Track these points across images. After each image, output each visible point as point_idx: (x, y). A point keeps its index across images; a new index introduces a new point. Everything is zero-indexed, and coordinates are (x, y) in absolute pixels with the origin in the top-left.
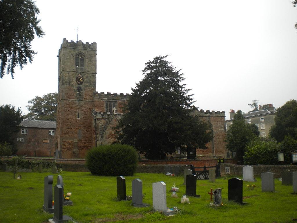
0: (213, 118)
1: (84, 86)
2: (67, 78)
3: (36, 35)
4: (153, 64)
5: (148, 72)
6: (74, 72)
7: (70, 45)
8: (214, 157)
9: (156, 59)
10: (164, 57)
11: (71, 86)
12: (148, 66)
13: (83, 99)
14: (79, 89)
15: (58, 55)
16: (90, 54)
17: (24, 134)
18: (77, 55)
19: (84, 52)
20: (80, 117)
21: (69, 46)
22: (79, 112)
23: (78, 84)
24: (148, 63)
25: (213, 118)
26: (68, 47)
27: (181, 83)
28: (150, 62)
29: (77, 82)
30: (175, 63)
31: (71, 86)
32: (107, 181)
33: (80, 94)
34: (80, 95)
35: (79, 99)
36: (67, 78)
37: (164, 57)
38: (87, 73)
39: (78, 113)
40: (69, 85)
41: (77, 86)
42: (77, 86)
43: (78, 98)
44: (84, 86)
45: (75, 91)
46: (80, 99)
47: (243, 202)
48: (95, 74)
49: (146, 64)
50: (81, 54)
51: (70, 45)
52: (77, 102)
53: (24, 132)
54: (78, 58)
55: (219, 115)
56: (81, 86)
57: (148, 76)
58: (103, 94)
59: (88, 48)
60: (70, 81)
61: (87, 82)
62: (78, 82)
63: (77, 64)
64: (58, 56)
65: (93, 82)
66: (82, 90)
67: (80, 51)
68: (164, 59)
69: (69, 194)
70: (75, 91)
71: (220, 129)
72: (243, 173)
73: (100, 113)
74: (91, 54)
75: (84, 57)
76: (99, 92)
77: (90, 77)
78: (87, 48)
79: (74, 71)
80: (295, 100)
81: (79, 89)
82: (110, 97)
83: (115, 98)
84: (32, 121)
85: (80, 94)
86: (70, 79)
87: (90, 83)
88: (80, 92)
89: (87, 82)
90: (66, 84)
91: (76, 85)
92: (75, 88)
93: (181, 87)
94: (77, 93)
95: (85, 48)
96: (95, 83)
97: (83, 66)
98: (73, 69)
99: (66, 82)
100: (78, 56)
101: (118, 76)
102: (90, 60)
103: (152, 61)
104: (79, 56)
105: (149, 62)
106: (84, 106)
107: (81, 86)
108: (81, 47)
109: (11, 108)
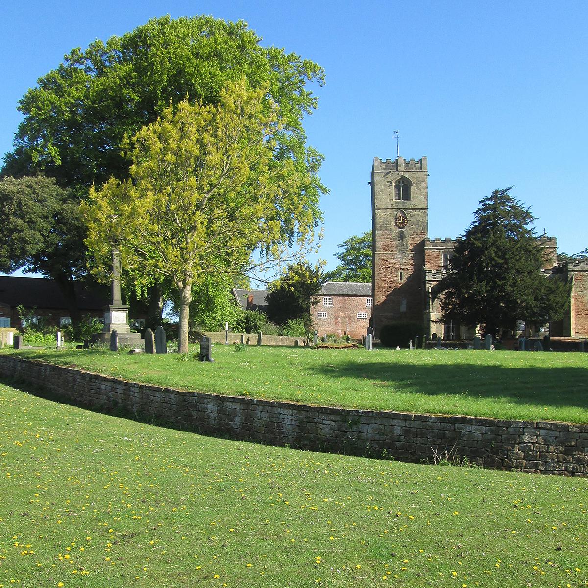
3: (95, 358)
7: (384, 167)
10: (506, 190)
13: (407, 251)
14: (402, 236)
17: (328, 305)
21: (384, 169)
23: (400, 228)
26: (383, 171)
28: (487, 199)
30: (521, 197)
32: (322, 386)
35: (401, 252)
36: (382, 220)
37: (506, 190)
40: (386, 230)
45: (394, 240)
46: (402, 251)
48: (426, 209)
49: (480, 202)
51: (384, 167)
52: (399, 256)
53: (328, 300)
56: (404, 230)
58: (438, 241)
62: (400, 225)
64: (369, 183)
65: (422, 223)
67: (402, 174)
81: (402, 236)
84: (340, 284)
88: (402, 240)
93: (528, 232)
95: (409, 169)
99: (381, 227)
101: (449, 219)
103: (489, 197)
104: (399, 182)
107: (404, 230)
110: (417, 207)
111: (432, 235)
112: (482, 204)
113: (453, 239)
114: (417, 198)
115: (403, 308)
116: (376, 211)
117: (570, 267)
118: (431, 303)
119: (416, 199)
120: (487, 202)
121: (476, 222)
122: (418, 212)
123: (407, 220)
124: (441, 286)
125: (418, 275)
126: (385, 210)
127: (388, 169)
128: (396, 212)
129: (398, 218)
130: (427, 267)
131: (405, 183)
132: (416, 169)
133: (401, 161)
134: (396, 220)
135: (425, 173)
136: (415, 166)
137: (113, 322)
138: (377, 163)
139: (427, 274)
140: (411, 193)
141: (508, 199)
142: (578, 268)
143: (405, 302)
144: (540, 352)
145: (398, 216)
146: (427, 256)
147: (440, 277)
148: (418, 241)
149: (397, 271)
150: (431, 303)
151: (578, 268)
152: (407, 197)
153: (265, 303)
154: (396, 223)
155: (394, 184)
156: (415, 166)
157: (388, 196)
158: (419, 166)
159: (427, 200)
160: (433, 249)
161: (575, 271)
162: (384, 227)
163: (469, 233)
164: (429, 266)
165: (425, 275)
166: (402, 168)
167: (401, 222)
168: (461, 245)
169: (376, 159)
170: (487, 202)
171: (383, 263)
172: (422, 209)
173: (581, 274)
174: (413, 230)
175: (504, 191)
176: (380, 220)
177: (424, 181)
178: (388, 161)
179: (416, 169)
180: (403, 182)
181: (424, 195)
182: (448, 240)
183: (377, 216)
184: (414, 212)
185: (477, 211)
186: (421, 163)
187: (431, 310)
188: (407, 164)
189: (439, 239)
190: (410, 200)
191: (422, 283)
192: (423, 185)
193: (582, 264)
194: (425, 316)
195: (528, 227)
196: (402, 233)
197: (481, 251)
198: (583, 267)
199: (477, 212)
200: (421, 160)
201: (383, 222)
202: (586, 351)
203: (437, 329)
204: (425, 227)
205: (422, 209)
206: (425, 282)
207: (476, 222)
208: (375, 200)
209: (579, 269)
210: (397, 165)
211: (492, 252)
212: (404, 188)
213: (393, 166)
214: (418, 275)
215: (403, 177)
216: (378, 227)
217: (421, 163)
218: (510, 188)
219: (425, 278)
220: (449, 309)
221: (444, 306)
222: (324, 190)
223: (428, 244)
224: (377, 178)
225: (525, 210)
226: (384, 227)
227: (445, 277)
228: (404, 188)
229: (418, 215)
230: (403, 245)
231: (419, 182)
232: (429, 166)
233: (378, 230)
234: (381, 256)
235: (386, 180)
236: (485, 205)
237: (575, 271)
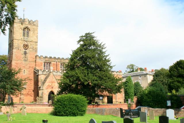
1: (29, 51)
2: (16, 44)
4: (84, 38)
5: (82, 43)
8: (117, 102)
9: (86, 34)
11: (19, 50)
12: (81, 39)
14: (25, 53)
18: (24, 29)
21: (19, 22)
22: (25, 69)
23: (25, 49)
27: (104, 50)
29: (24, 48)
30: (100, 38)
31: (19, 50)
33: (26, 56)
34: (26, 57)
40: (18, 49)
43: (24, 59)
44: (28, 51)
45: (22, 54)
49: (80, 37)
50: (27, 28)
56: (26, 50)
57: (82, 46)
59: (32, 24)
61: (31, 48)
63: (24, 35)
64: (9, 29)
65: (35, 48)
66: (27, 54)
67: (27, 25)
68: (92, 35)
70: (22, 54)
72: (71, 116)
73: (41, 70)
77: (33, 45)
80: (170, 66)
81: (25, 53)
82: (47, 59)
83: (50, 60)
85: (26, 56)
86: (19, 45)
88: (26, 55)
89: (31, 48)
90: (16, 49)
91: (23, 50)
92: (23, 53)
94: (23, 56)
95: (30, 24)
96: (36, 49)
97: (28, 36)
98: (21, 39)
99: (16, 48)
102: (34, 33)
103: (83, 35)
106: (28, 65)
108: (27, 23)
111: (39, 54)
119: (32, 36)
126: (18, 40)
137: (135, 105)
144: (79, 116)
167: (26, 46)
174: (31, 51)
175: (91, 33)
177: (37, 30)
181: (36, 36)
188: (29, 22)
192: (36, 32)
196: (26, 52)
202: (124, 122)
204: (36, 50)
230: (26, 57)
234: (15, 62)
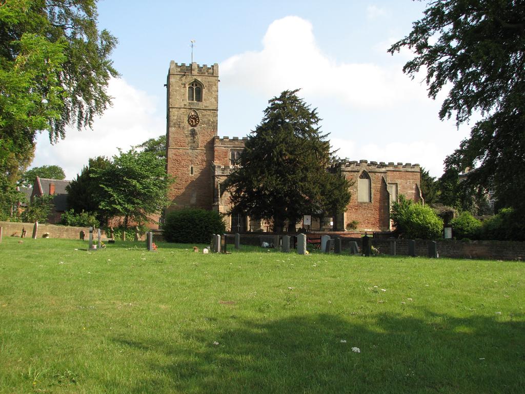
0: (399, 174)
6: (185, 109)
9: (284, 93)
10: (294, 92)
14: (193, 133)
15: (166, 84)
16: (208, 82)
19: (199, 80)
20: (194, 173)
21: (179, 72)
24: (273, 100)
25: (399, 174)
28: (276, 99)
30: (308, 98)
37: (294, 92)
38: (203, 110)
39: (192, 168)
40: (179, 127)
41: (191, 128)
42: (191, 128)
47: (85, 239)
49: (270, 101)
52: (190, 151)
54: (194, 86)
55: (410, 170)
56: (195, 128)
58: (227, 140)
60: (179, 122)
64: (165, 85)
65: (213, 122)
67: (195, 77)
69: (109, 260)
71: (409, 192)
74: (211, 82)
75: (201, 87)
76: (221, 137)
78: (205, 73)
79: (185, 107)
81: (193, 133)
82: (236, 143)
87: (208, 124)
88: (194, 138)
90: (175, 127)
92: (187, 133)
94: (189, 139)
95: (202, 73)
99: (174, 124)
100: (191, 86)
101: (239, 118)
104: (193, 85)
105: (274, 98)
109: (105, 160)
110: (208, 108)
111: (221, 134)
112: (271, 103)
113: (240, 138)
114: (209, 100)
115: (193, 200)
116: (171, 110)
117: (343, 167)
118: (219, 196)
120: (276, 102)
121: (266, 119)
122: (208, 112)
123: (198, 119)
124: (232, 179)
125: (209, 172)
126: (178, 109)
127: (183, 72)
128: (189, 111)
129: (191, 117)
130: (216, 163)
131: (198, 86)
132: (208, 74)
133: (195, 67)
134: (189, 119)
135: (216, 78)
136: (208, 72)
138: (173, 66)
139: (216, 169)
140: (203, 95)
141: (295, 100)
142: (349, 169)
143: (194, 195)
145: (190, 115)
146: (216, 153)
147: (228, 172)
148: (209, 139)
149: (188, 166)
150: (219, 196)
151: (349, 169)
152: (199, 99)
153: (66, 192)
154: (189, 121)
155: (187, 87)
156: (208, 72)
157: (182, 96)
158: (211, 72)
159: (217, 102)
160: (221, 146)
161: (346, 171)
162: (177, 124)
163: (260, 130)
164: (218, 162)
165: (214, 170)
166: (195, 72)
167: (194, 120)
168: (250, 142)
169: (172, 62)
170: (276, 102)
171: (175, 157)
172: (213, 110)
173: (352, 174)
176: (174, 118)
177: (215, 85)
178: (183, 65)
179: (208, 74)
180: (196, 85)
182: (235, 139)
183: (171, 114)
184: (205, 112)
185: (267, 109)
186: (213, 69)
187: (220, 202)
188: (200, 69)
189: (227, 138)
190: (202, 101)
191: (212, 178)
192: (214, 88)
193: (352, 166)
194: (214, 208)
195: (314, 126)
196: (194, 130)
197: (274, 145)
198: (353, 168)
199: (266, 111)
200: (213, 66)
201: (177, 120)
203: (438, 257)
204: (215, 127)
205: (213, 110)
206: (214, 177)
207: (266, 119)
208: (170, 100)
209: (351, 170)
210: (191, 70)
211: (283, 147)
212: (197, 91)
213: (187, 70)
214: (209, 172)
215: (196, 81)
216: (172, 124)
217: (213, 69)
218: (297, 91)
219: (214, 173)
220: (238, 202)
221: (234, 199)
222: (115, 73)
223: (217, 142)
224: (172, 80)
225: (311, 112)
226: (177, 124)
227: (233, 172)
228: (197, 91)
229: (209, 115)
231: (210, 86)
232: (222, 72)
233: (172, 127)
234: (174, 151)
235: (180, 82)
236: (274, 104)
237: (346, 171)
